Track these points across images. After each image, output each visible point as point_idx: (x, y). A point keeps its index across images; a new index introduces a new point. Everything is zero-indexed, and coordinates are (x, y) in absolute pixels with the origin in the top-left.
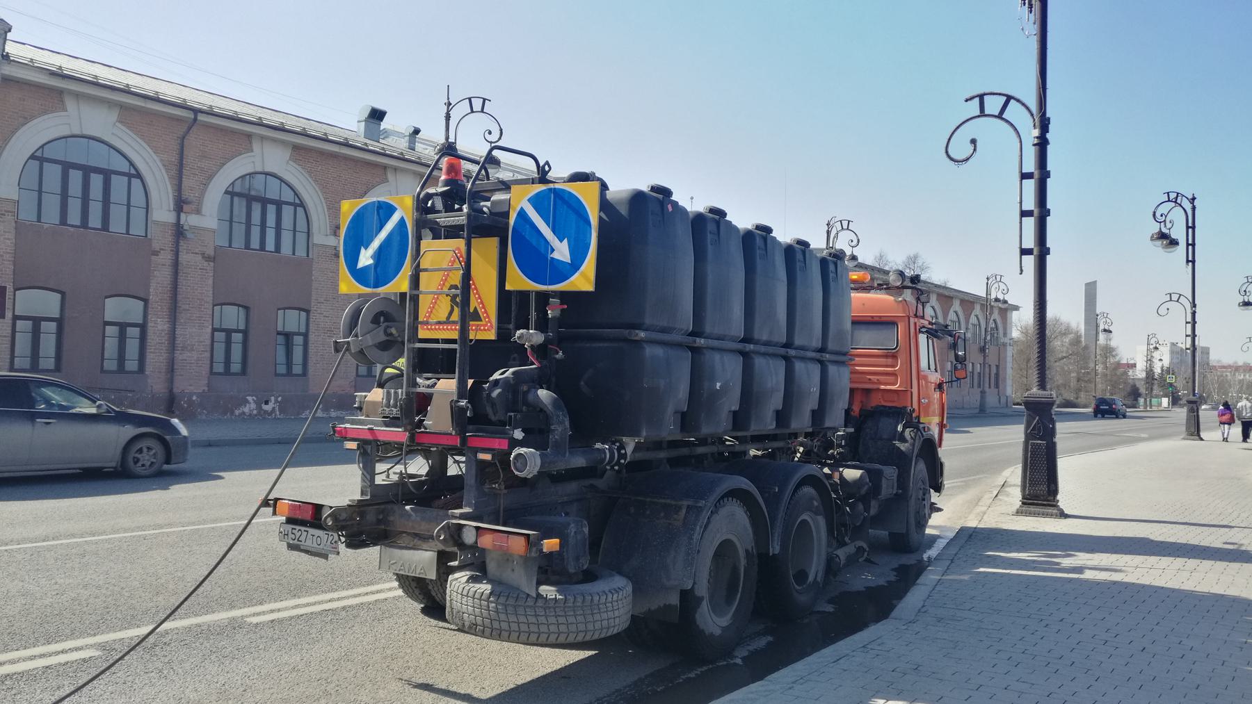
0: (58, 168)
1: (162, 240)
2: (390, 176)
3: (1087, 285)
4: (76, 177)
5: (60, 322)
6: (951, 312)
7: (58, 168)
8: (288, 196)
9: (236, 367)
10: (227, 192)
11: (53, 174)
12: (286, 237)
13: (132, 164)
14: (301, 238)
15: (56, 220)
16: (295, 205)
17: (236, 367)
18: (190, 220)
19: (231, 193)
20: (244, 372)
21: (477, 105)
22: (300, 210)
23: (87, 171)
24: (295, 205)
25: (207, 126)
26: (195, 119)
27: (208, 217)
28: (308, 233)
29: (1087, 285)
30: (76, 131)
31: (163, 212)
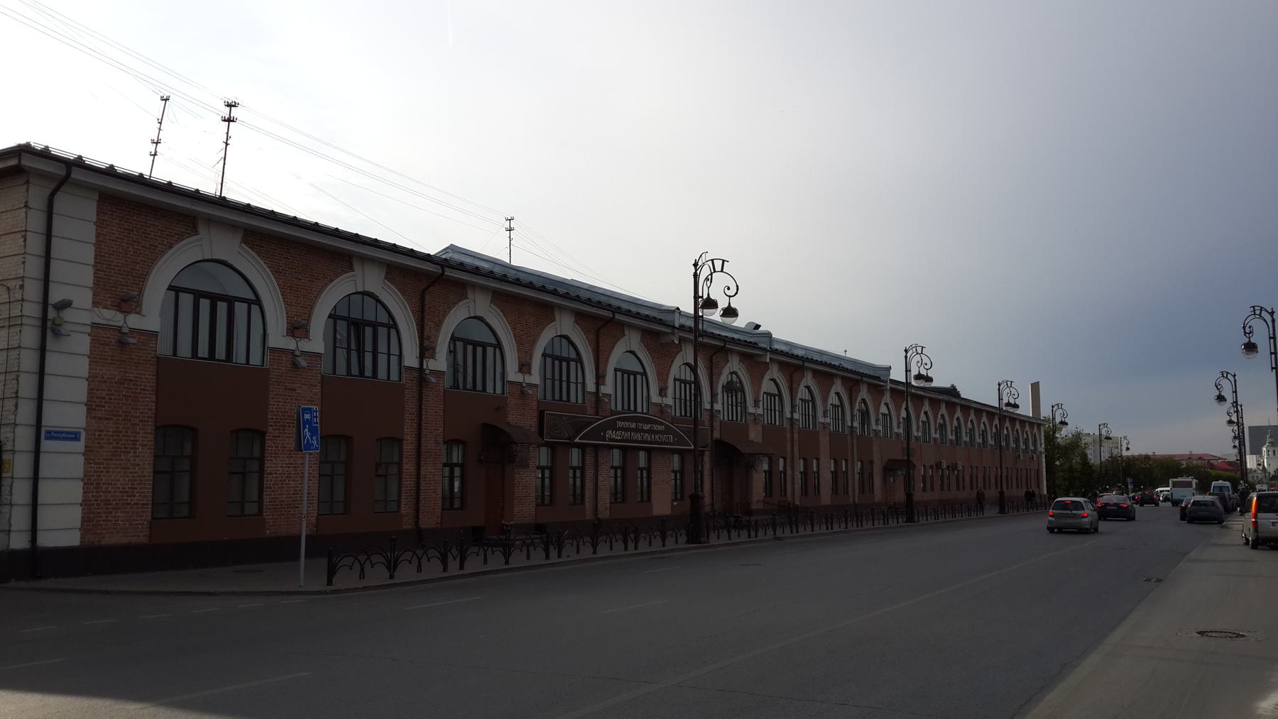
0: (191, 296)
1: (786, 424)
2: (356, 266)
3: (1183, 518)
4: (205, 304)
5: (552, 469)
6: (802, 387)
7: (191, 296)
8: (383, 318)
9: (547, 501)
10: (330, 316)
12: (382, 359)
13: (391, 316)
14: (394, 360)
16: (249, 302)
17: (547, 501)
18: (431, 365)
19: (333, 316)
20: (462, 507)
21: (718, 265)
22: (255, 308)
23: (214, 299)
24: (249, 302)
25: (80, 185)
26: (69, 174)
27: (440, 362)
28: (400, 356)
29: (1183, 518)
31: (411, 360)
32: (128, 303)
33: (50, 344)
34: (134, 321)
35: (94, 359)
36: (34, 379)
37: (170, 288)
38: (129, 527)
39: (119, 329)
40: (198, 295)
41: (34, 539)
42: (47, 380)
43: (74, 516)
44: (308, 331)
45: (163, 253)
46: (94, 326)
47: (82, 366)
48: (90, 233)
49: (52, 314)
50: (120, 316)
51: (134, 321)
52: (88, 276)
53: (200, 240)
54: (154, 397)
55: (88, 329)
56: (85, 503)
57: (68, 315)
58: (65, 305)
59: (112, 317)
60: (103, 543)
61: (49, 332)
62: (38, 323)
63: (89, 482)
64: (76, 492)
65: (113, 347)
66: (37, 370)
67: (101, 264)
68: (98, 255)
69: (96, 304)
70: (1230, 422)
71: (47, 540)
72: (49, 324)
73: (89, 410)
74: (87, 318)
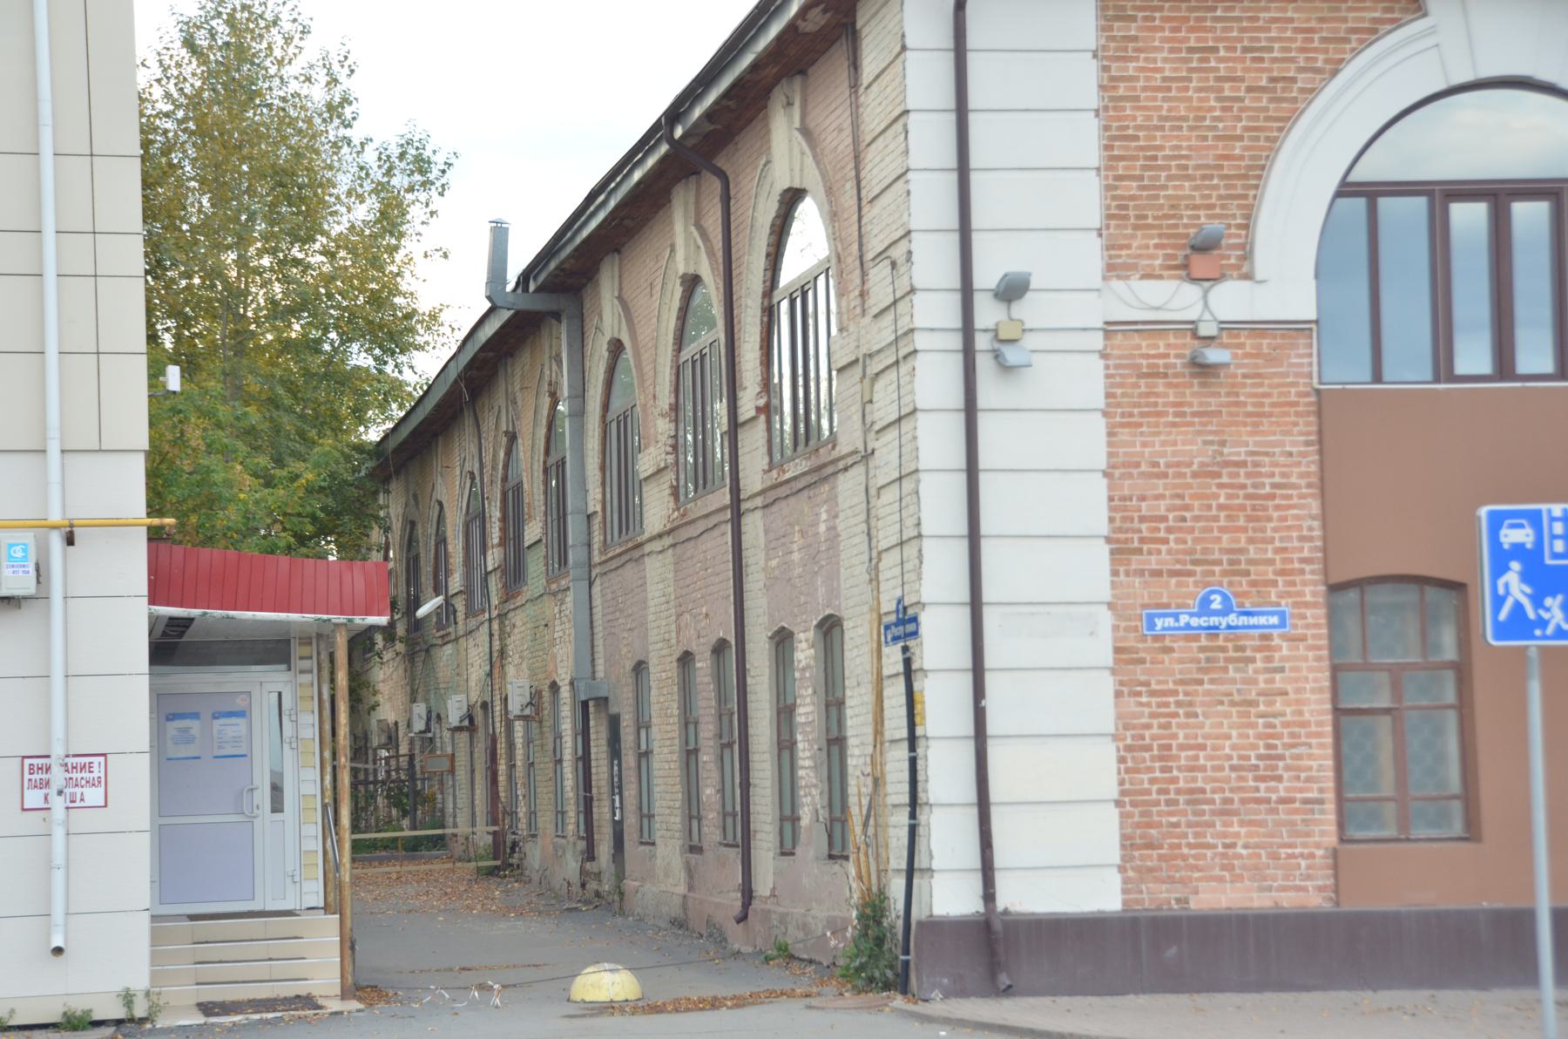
11: (1404, 218)
15: (1484, 366)
30: (1468, 77)
32: (1205, 255)
33: (988, 393)
34: (1231, 301)
35: (1122, 414)
36: (955, 425)
37: (1346, 189)
38: (1279, 865)
39: (1192, 329)
40: (1443, 195)
41: (989, 896)
42: (987, 547)
43: (1102, 833)
44: (1247, 254)
45: (1312, 92)
46: (1111, 329)
47: (1089, 441)
48: (1081, 81)
49: (987, 313)
50: (1191, 292)
51: (1231, 301)
52: (1086, 200)
53: (1432, 30)
54: (1314, 506)
55: (1098, 341)
56: (1129, 799)
57: (1028, 310)
58: (1012, 290)
59: (1175, 299)
60: (1193, 905)
61: (984, 363)
62: (956, 341)
63: (1136, 748)
64: (1100, 770)
65: (1165, 377)
66: (963, 464)
67: (1124, 153)
68: (1116, 142)
69: (1113, 269)
70: (1012, 290)
71: (1021, 896)
72: (982, 342)
73: (1120, 552)
74: (1096, 309)
